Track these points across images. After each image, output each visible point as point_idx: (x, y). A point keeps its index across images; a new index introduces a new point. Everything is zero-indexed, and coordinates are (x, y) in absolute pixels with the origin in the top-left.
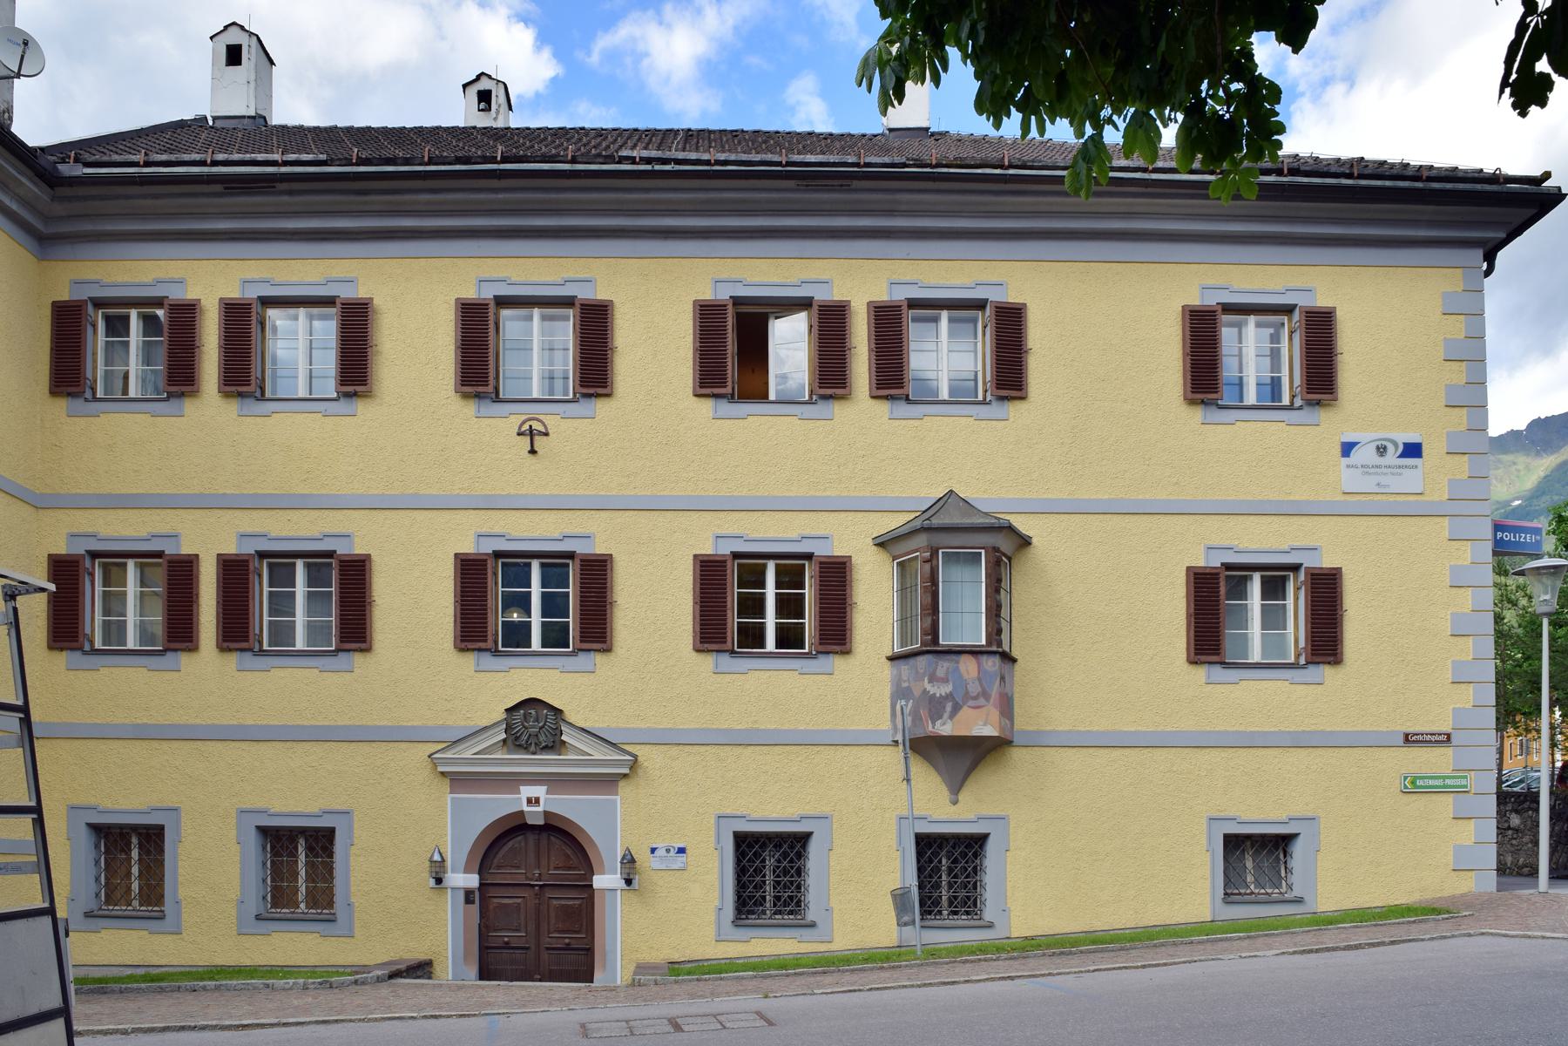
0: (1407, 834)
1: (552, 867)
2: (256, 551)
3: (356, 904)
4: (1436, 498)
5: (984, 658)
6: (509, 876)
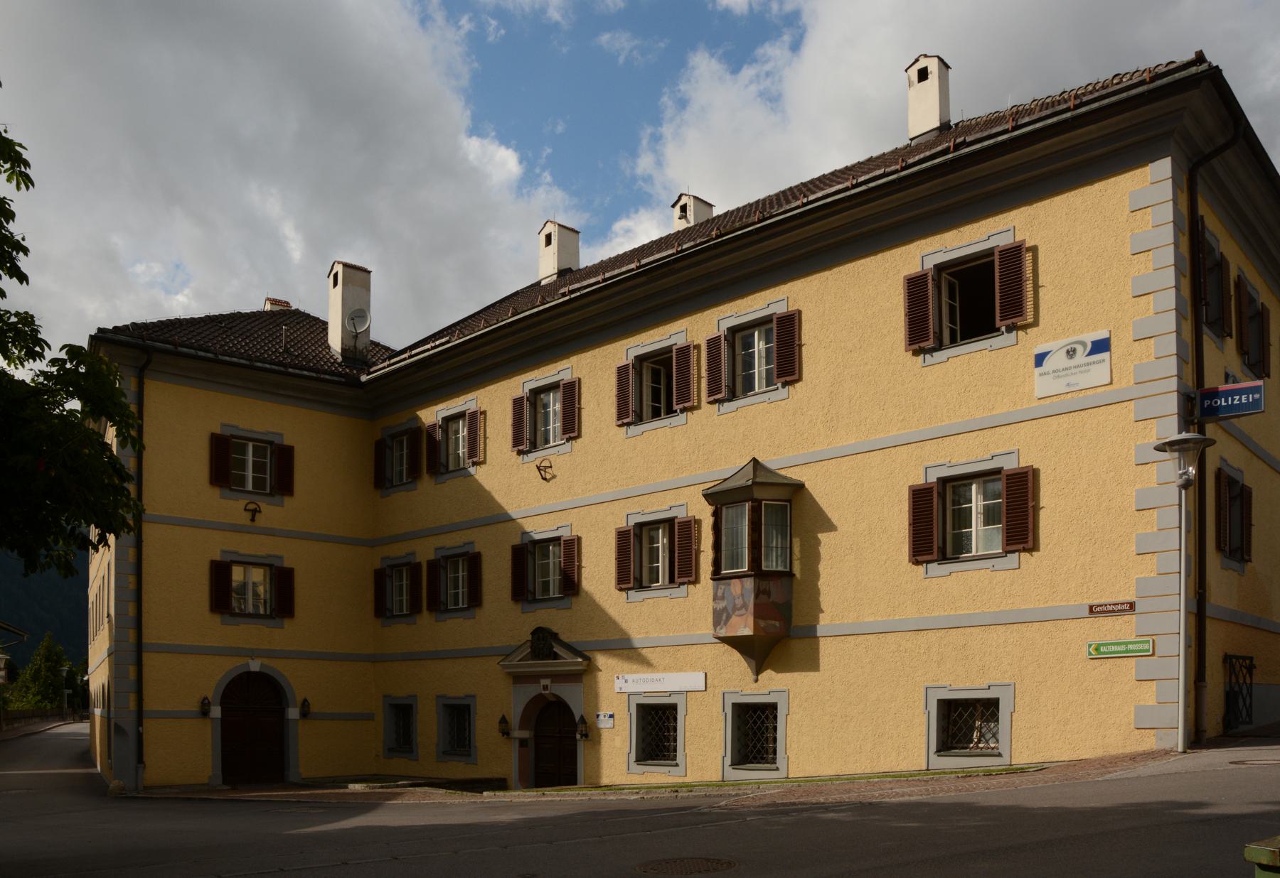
5: (745, 580)
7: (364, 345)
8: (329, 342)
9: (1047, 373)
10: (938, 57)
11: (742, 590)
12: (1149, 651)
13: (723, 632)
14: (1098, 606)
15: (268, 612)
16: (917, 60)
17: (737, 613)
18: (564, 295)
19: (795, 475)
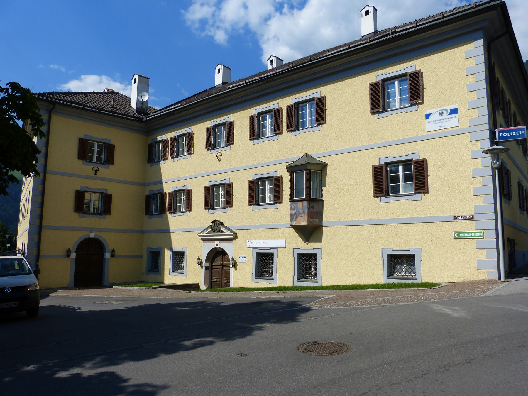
0: (457, 255)
1: (225, 261)
2: (384, 163)
4: (465, 126)
7: (146, 107)
8: (131, 105)
9: (431, 122)
10: (373, 6)
11: (303, 206)
12: (482, 237)
13: (294, 223)
14: (458, 217)
15: (100, 212)
16: (365, 8)
17: (301, 215)
18: (229, 88)
19: (323, 160)
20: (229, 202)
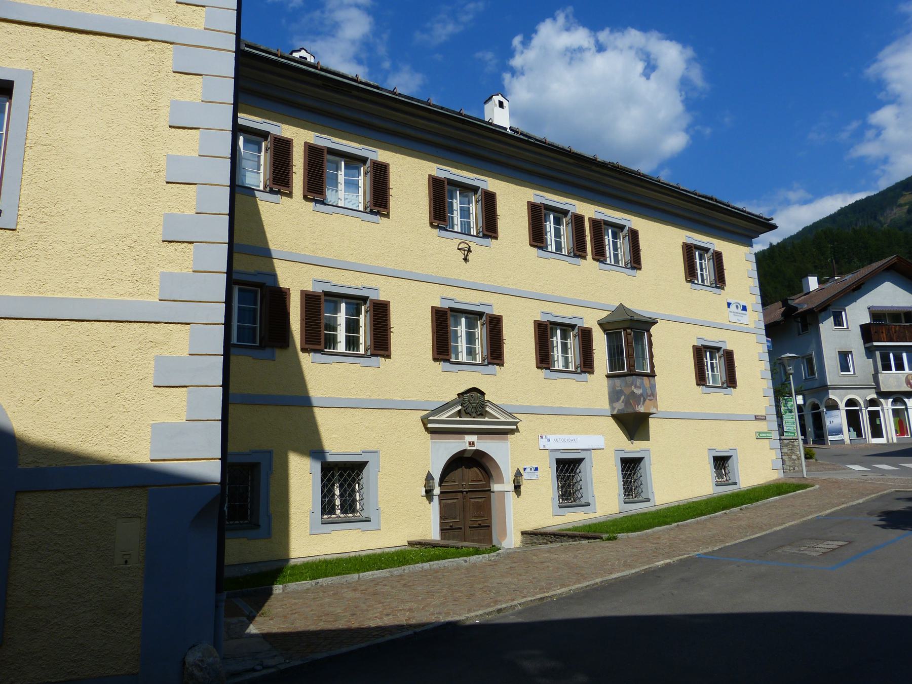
3: (382, 509)
6: (450, 487)
17: (649, 398)
20: (495, 355)
